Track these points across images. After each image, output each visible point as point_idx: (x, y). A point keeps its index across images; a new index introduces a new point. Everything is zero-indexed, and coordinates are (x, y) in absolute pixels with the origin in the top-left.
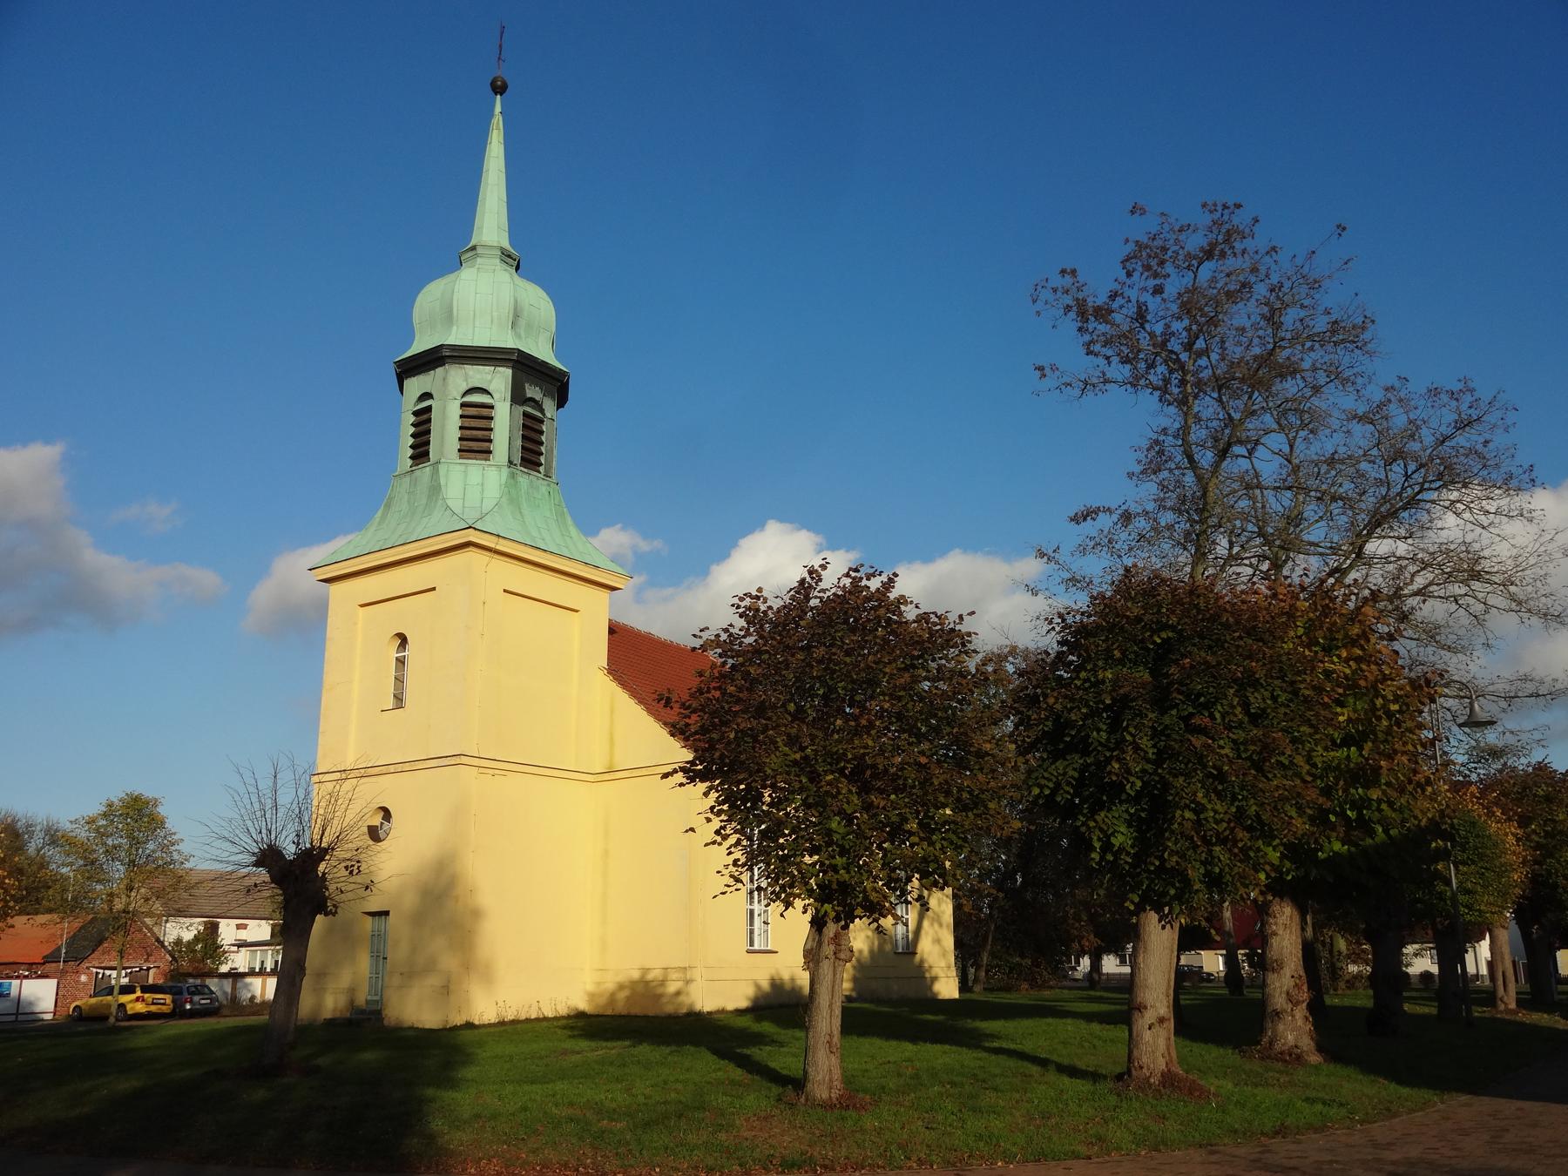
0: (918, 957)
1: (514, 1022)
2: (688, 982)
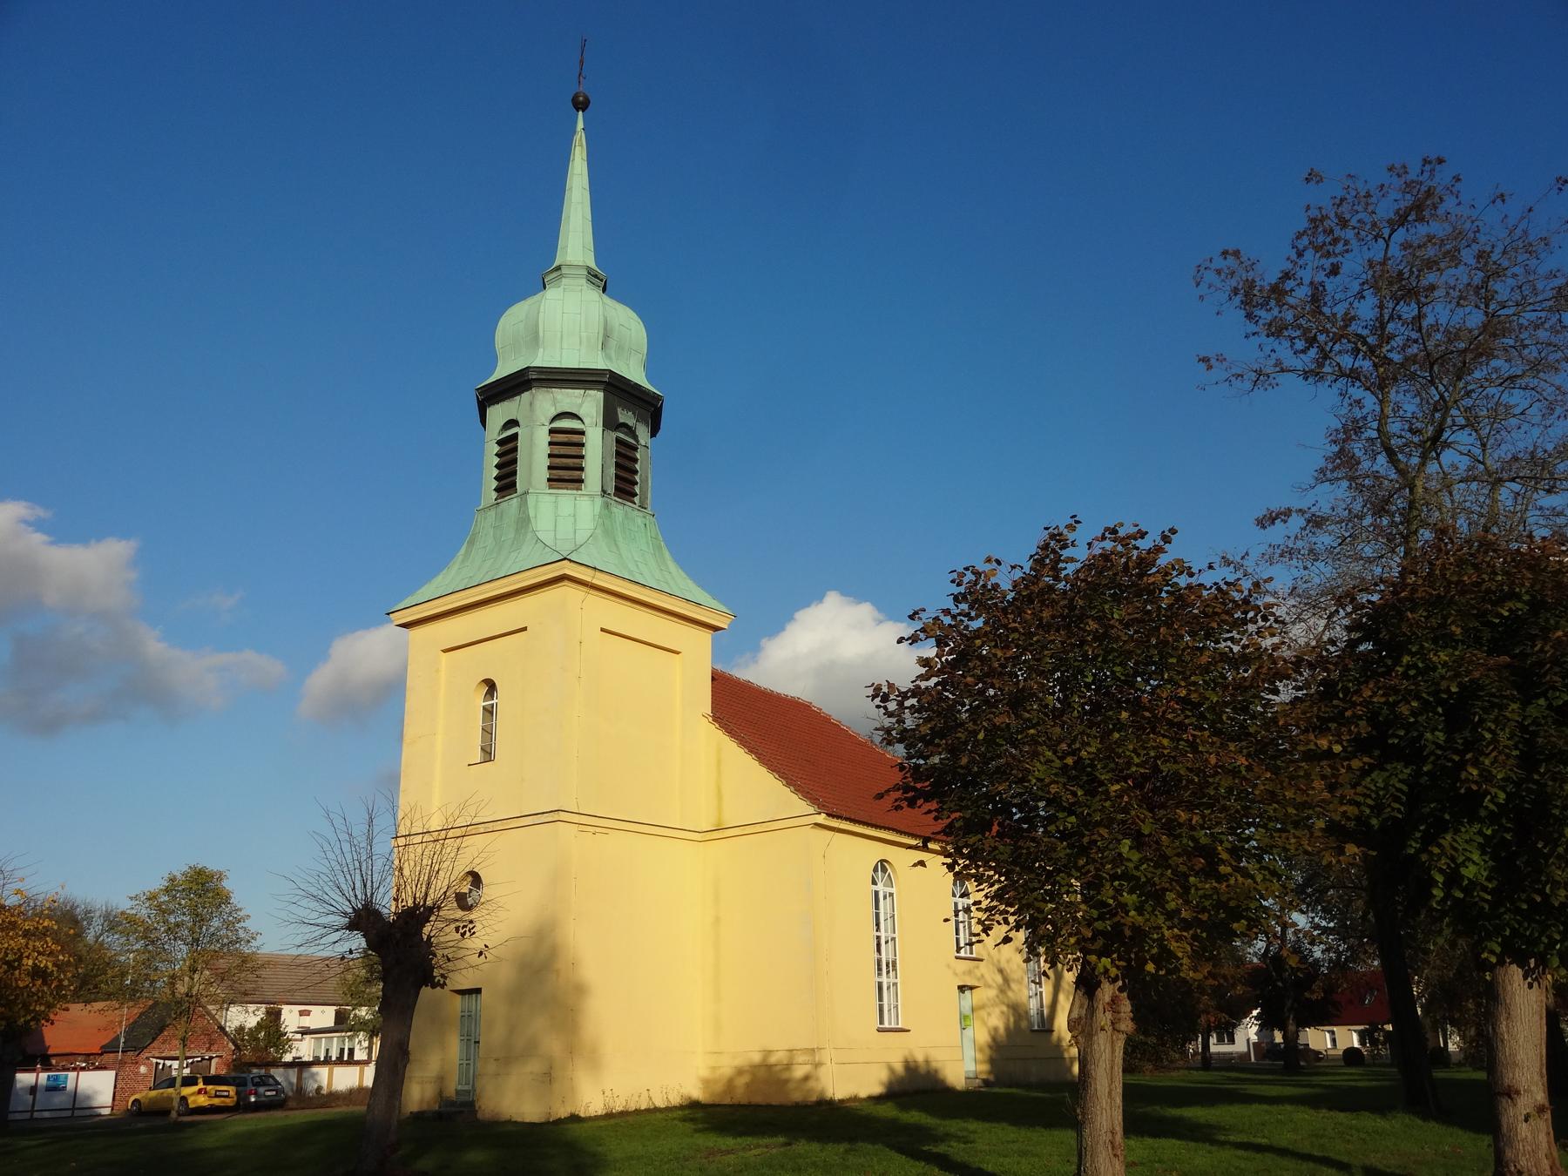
0: (1055, 1035)
2: (818, 1065)
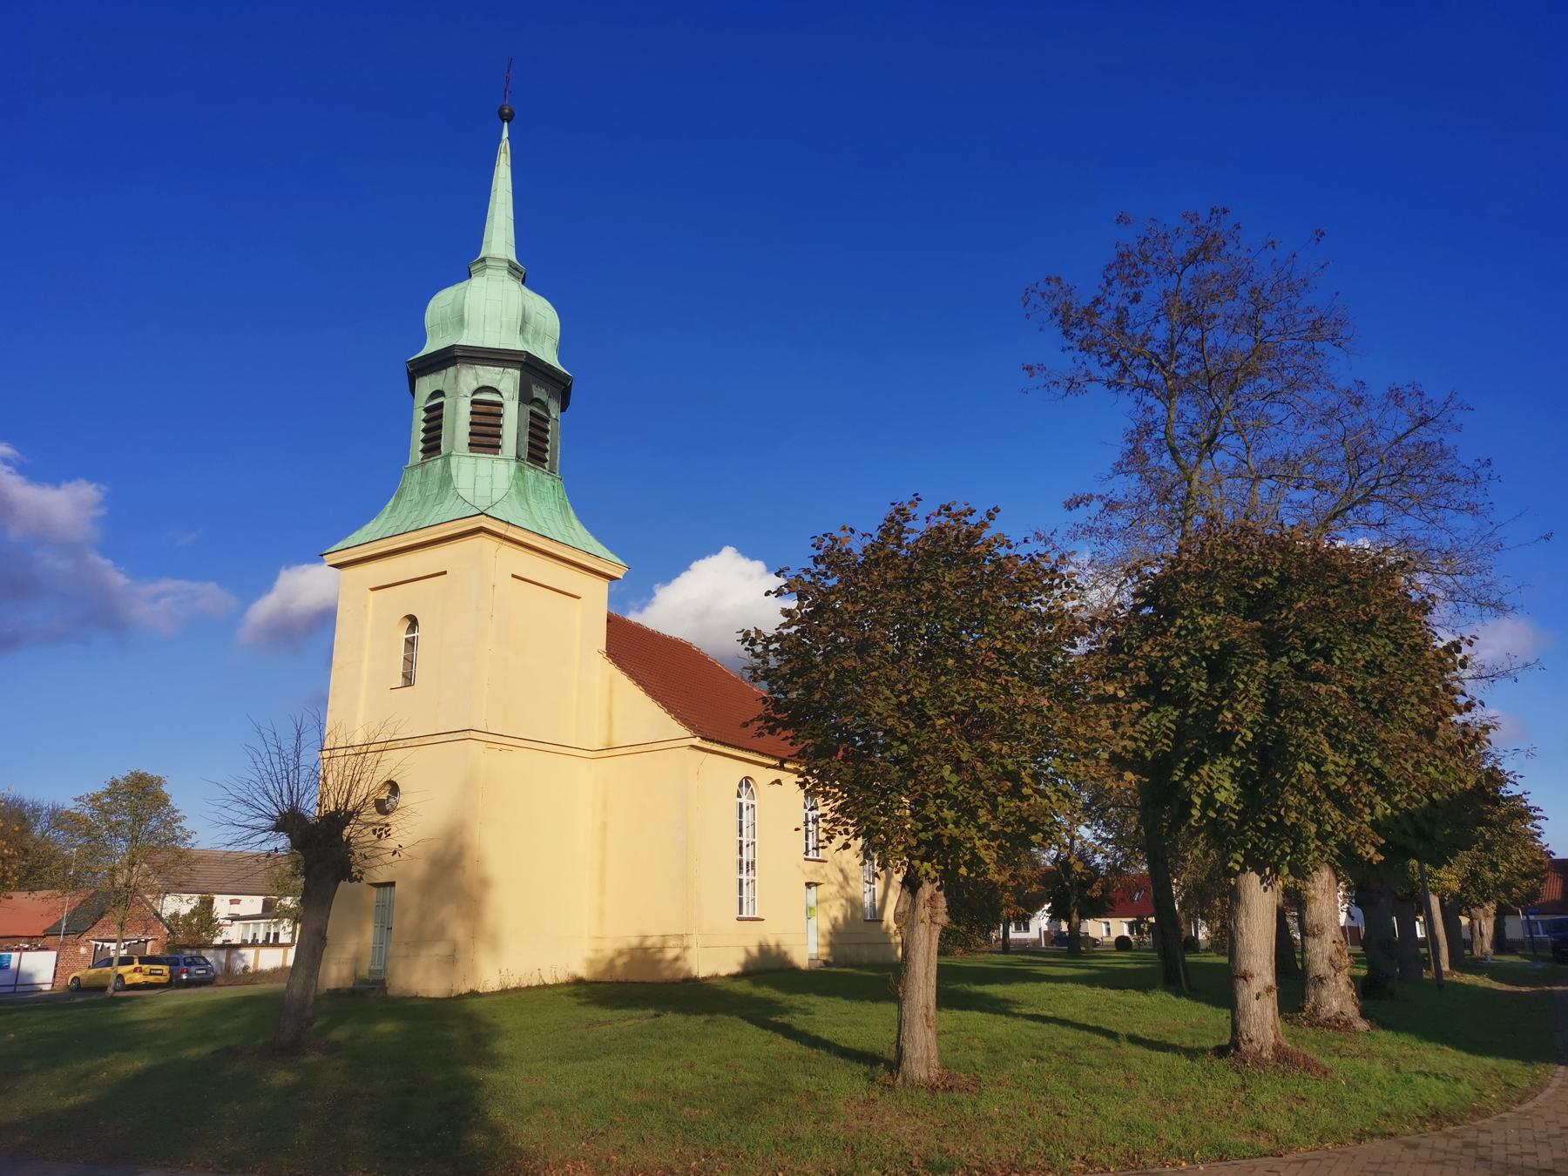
1: (517, 990)
2: (686, 948)
